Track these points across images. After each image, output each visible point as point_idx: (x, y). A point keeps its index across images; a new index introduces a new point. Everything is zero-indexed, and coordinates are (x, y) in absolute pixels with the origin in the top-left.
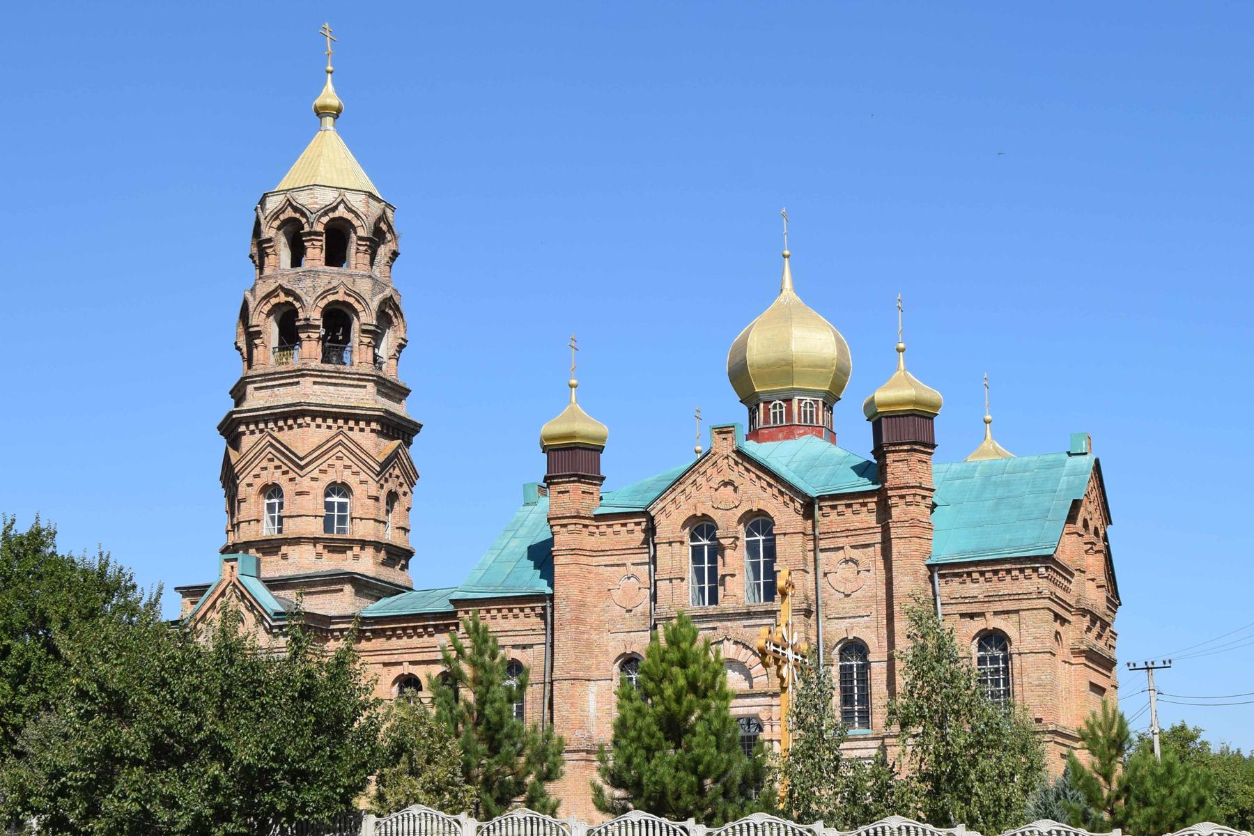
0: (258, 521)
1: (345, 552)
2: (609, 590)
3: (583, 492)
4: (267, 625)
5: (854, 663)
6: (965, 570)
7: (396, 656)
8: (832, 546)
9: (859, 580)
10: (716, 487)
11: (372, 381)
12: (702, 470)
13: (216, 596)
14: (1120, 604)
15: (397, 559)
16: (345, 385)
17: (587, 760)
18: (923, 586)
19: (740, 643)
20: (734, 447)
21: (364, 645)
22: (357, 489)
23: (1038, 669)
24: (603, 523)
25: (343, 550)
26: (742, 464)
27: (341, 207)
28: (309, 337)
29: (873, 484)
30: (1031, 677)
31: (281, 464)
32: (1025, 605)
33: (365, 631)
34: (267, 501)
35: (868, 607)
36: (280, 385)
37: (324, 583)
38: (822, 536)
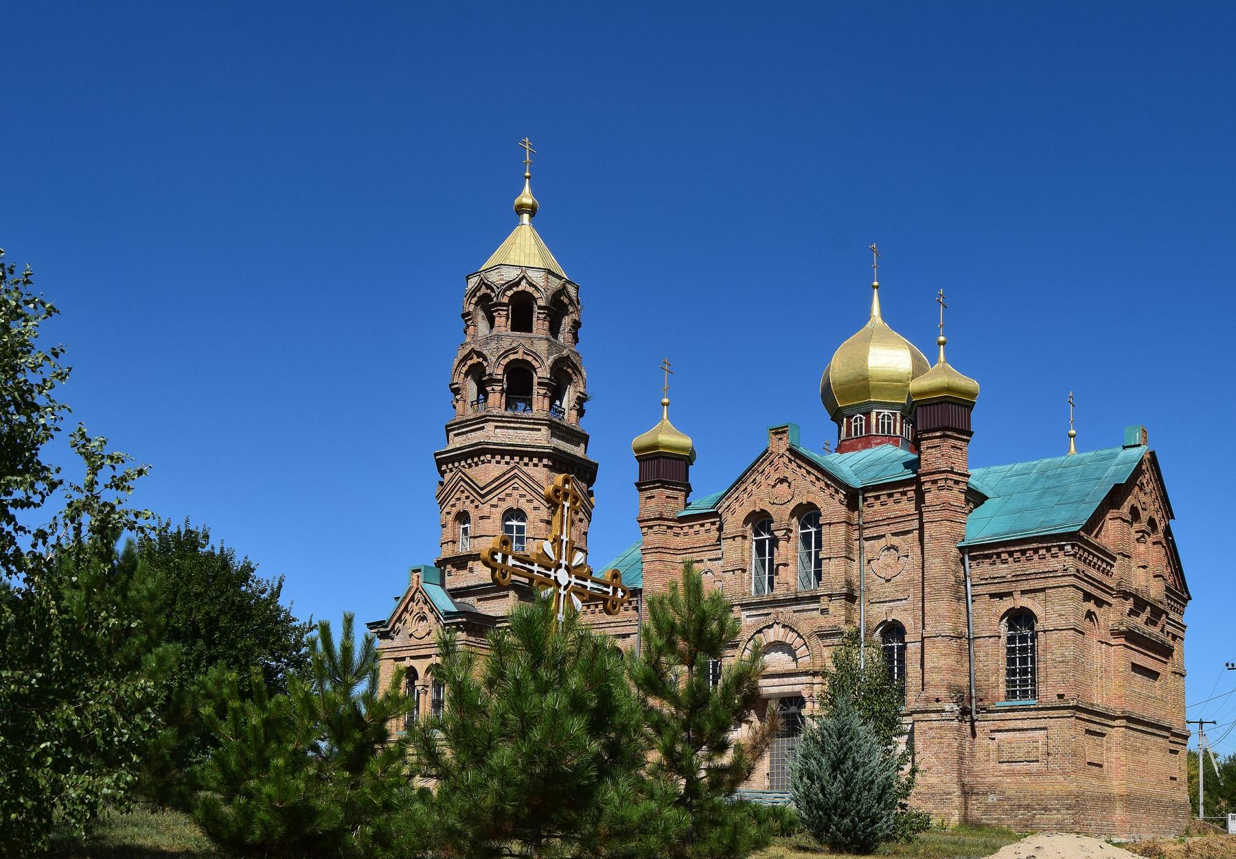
0: (454, 542)
3: (668, 497)
5: (895, 644)
6: (994, 551)
8: (875, 535)
12: (761, 469)
13: (407, 600)
14: (1190, 598)
18: (953, 567)
19: (787, 626)
22: (531, 515)
24: (686, 524)
26: (794, 461)
27: (524, 282)
28: (493, 389)
32: (1051, 583)
34: (462, 526)
35: (905, 590)
38: (866, 526)
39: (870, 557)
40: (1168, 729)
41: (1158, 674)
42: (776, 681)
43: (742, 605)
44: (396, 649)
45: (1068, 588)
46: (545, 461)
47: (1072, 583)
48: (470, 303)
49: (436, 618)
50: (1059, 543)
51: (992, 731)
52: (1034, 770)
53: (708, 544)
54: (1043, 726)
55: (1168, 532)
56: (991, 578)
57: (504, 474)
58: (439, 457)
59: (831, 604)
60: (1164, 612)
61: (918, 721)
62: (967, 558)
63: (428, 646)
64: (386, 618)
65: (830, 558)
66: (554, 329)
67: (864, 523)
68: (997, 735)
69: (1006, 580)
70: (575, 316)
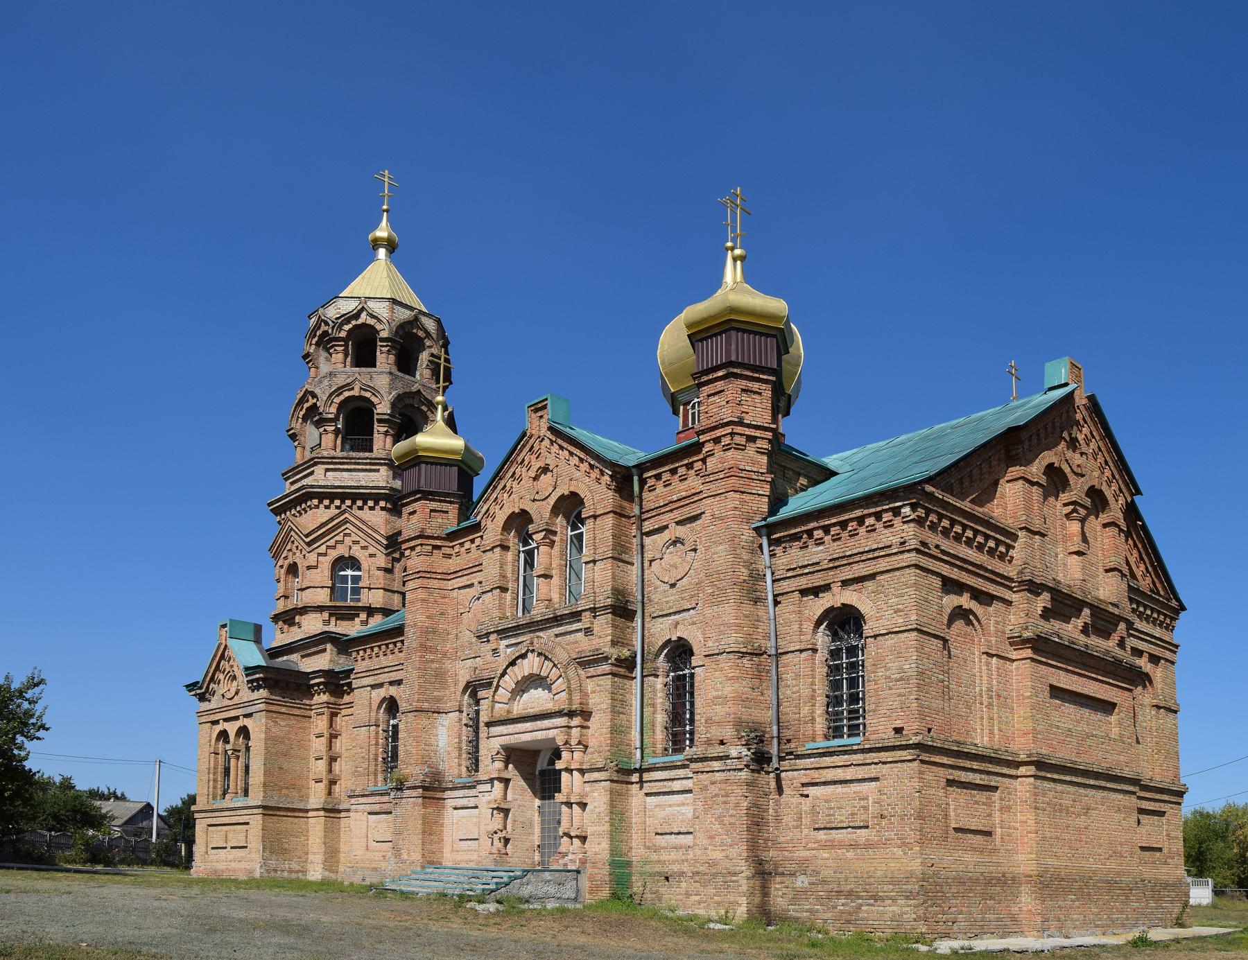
1: (353, 619)
6: (804, 528)
11: (385, 464)
12: (519, 459)
13: (217, 659)
14: (1183, 608)
23: (899, 655)
25: (351, 618)
26: (555, 442)
27: (364, 315)
28: (325, 430)
32: (883, 565)
33: (343, 685)
40: (1135, 782)
41: (1114, 705)
42: (529, 726)
43: (498, 632)
45: (907, 571)
46: (382, 504)
47: (913, 563)
51: (803, 785)
52: (862, 840)
54: (872, 776)
55: (1132, 512)
57: (332, 519)
59: (596, 622)
60: (1120, 618)
62: (765, 541)
64: (200, 679)
68: (811, 791)
69: (820, 568)
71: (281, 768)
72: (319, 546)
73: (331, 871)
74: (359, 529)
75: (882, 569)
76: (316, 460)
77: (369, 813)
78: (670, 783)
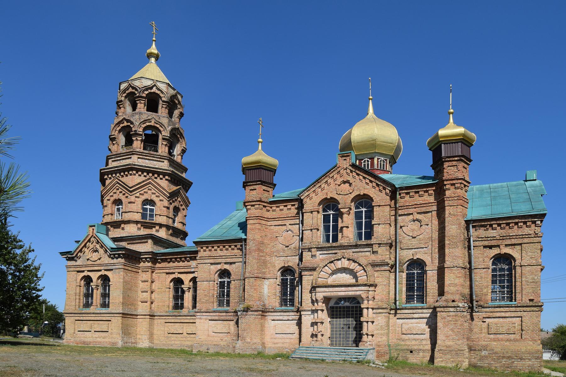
1: (152, 229)
2: (276, 237)
3: (264, 190)
4: (108, 253)
5: (415, 272)
6: (489, 223)
7: (172, 270)
8: (406, 213)
9: (421, 230)
10: (339, 184)
12: (331, 176)
13: (86, 241)
15: (179, 235)
16: (154, 160)
17: (262, 315)
19: (351, 260)
20: (351, 163)
21: (158, 265)
22: (158, 203)
23: (532, 273)
24: (274, 205)
25: (151, 228)
26: (355, 172)
27: (154, 88)
28: (137, 139)
29: (432, 181)
30: (528, 278)
31: (122, 191)
32: (526, 240)
33: (158, 259)
34: (117, 207)
36: (123, 159)
37: (139, 239)
38: (400, 208)
39: (402, 225)
42: (343, 289)
43: (317, 248)
44: (78, 266)
45: (537, 244)
48: (122, 96)
49: (104, 251)
50: (532, 220)
51: (484, 318)
52: (512, 339)
53: (290, 216)
56: (486, 237)
57: (144, 181)
58: (103, 171)
61: (440, 312)
63: (99, 265)
64: (72, 250)
65: (379, 224)
66: (171, 114)
67: (399, 207)
70: (181, 110)
71: (128, 296)
72: (136, 193)
73: (152, 343)
74: (156, 187)
75: (526, 242)
76: (134, 152)
77: (209, 320)
78: (412, 315)
